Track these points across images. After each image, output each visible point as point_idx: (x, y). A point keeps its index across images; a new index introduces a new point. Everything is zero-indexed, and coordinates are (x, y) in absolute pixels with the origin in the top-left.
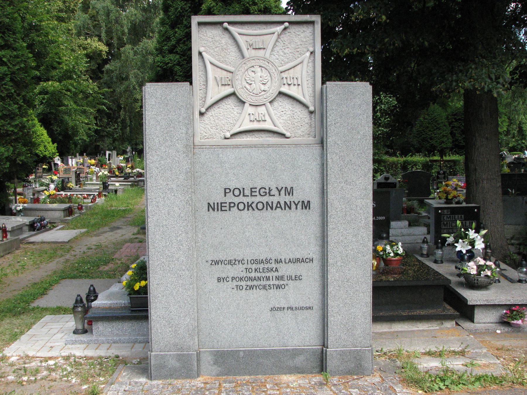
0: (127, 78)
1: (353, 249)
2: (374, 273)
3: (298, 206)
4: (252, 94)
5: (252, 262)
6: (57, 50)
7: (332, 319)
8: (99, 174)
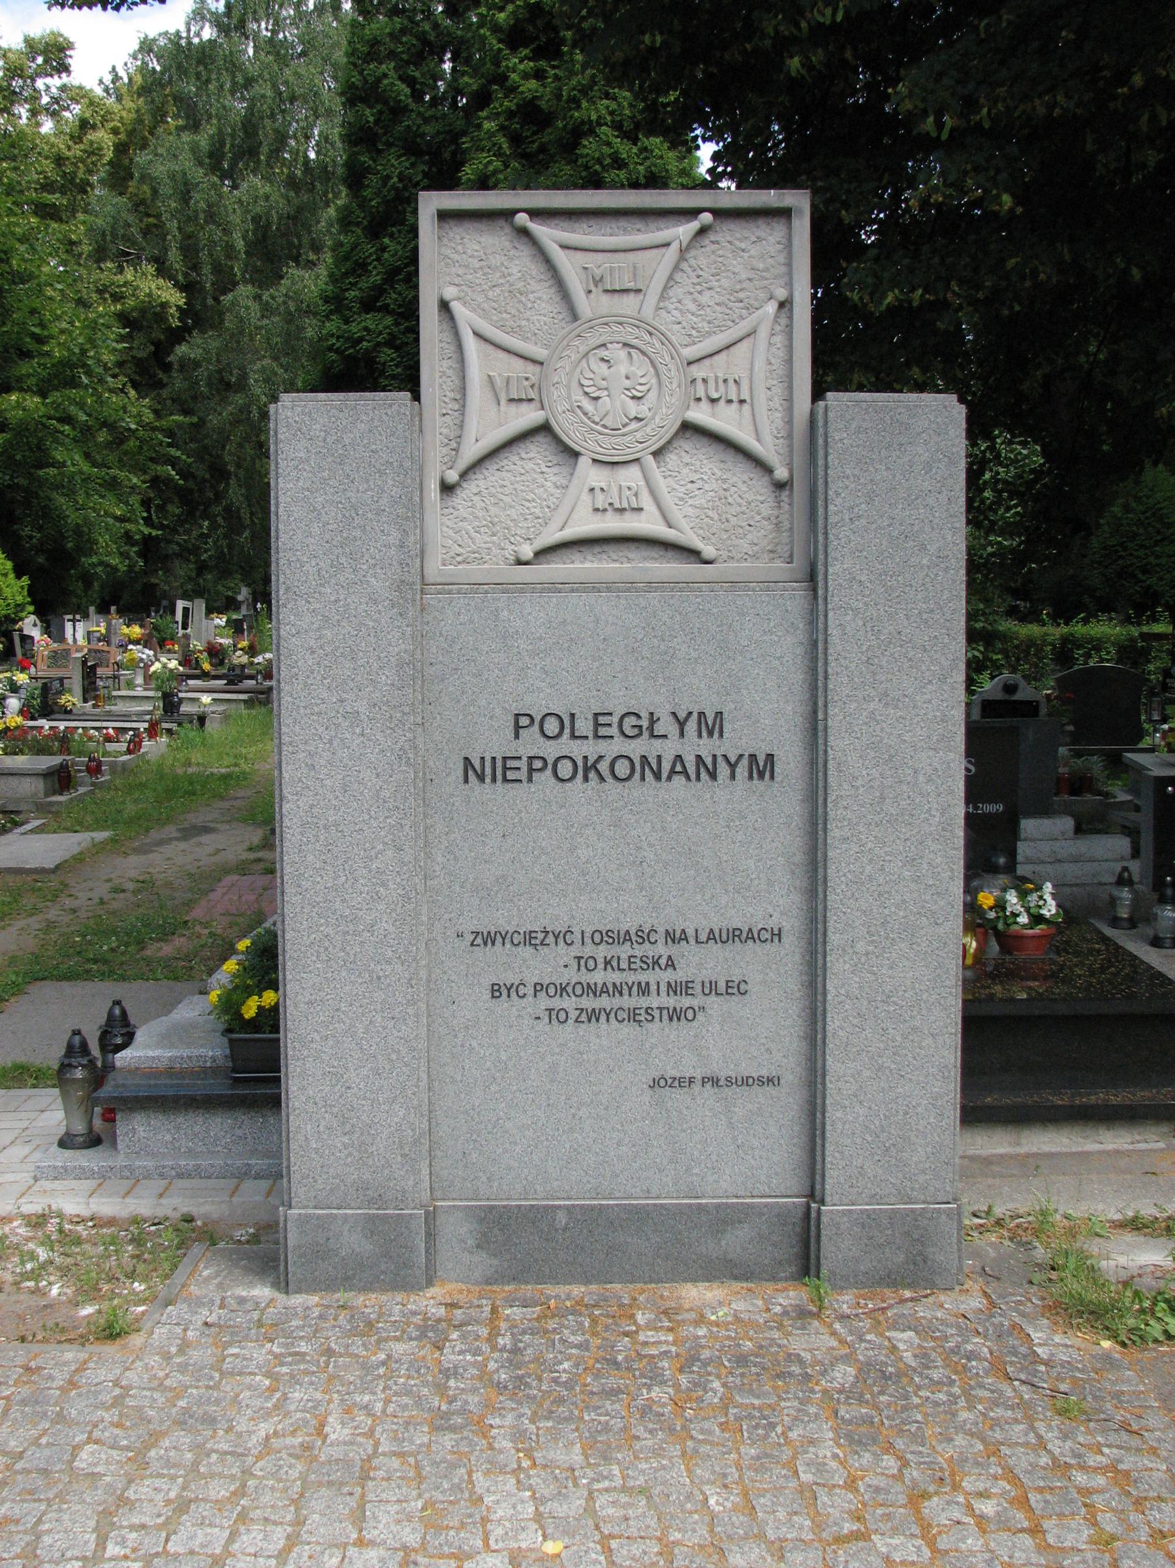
0: (242, 385)
1: (904, 901)
2: (969, 974)
3: (738, 770)
4: (598, 428)
5: (597, 937)
6: (37, 304)
7: (839, 1114)
8: (152, 669)
